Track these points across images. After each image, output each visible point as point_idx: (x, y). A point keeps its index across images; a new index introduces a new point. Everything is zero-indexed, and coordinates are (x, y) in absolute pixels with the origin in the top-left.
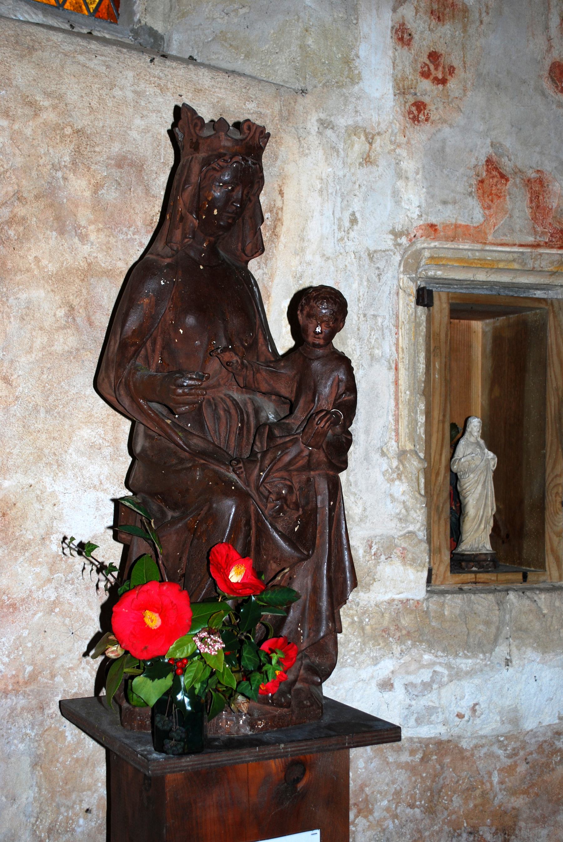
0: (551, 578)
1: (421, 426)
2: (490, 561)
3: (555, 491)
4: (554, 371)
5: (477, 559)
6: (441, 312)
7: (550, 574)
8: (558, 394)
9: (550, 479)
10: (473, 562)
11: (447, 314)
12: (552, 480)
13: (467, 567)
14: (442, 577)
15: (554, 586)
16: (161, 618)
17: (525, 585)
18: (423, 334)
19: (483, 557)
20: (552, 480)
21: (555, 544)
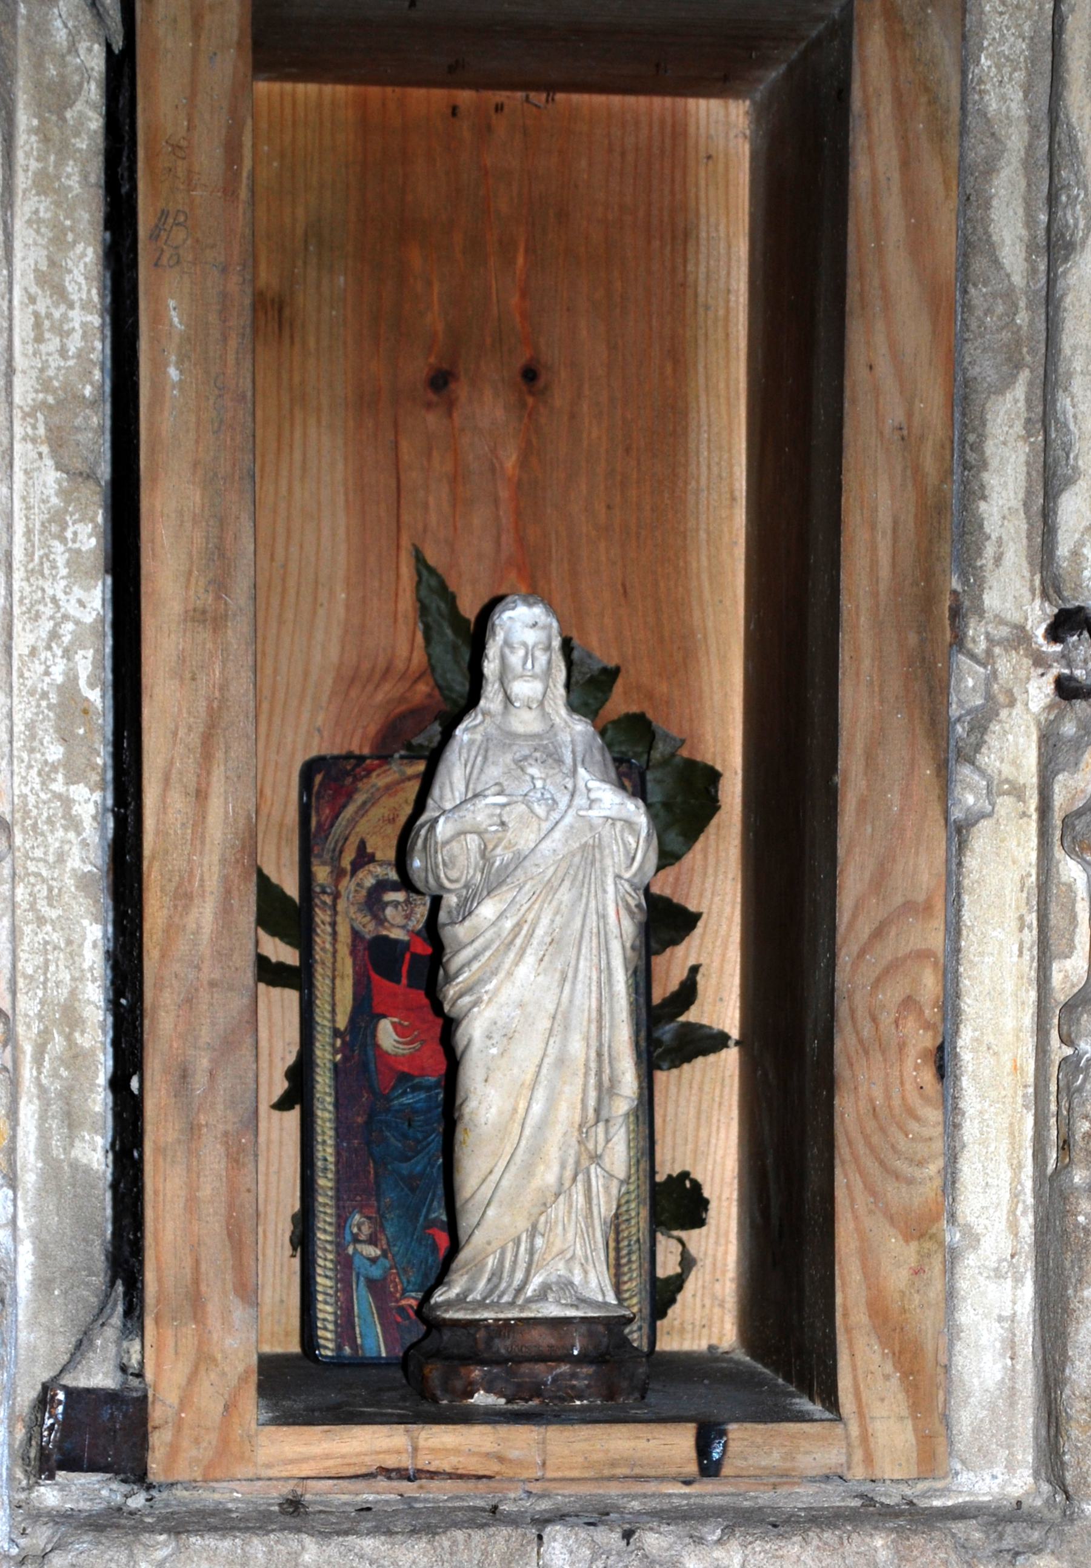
0: (869, 1460)
1: (78, 642)
2: (584, 1359)
3: (891, 995)
4: (892, 345)
5: (502, 1346)
6: (197, 23)
7: (865, 1438)
8: (917, 469)
9: (865, 929)
10: (482, 1362)
11: (234, 34)
12: (878, 934)
13: (447, 1390)
14: (212, 1438)
15: (868, 1500)
16: (696, 1057)
17: (708, 1491)
18: (82, 144)
19: (542, 1339)
20: (878, 934)
21: (897, 1278)
